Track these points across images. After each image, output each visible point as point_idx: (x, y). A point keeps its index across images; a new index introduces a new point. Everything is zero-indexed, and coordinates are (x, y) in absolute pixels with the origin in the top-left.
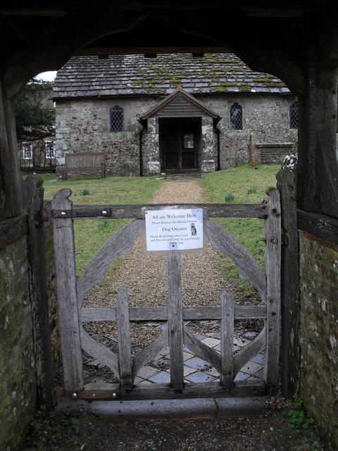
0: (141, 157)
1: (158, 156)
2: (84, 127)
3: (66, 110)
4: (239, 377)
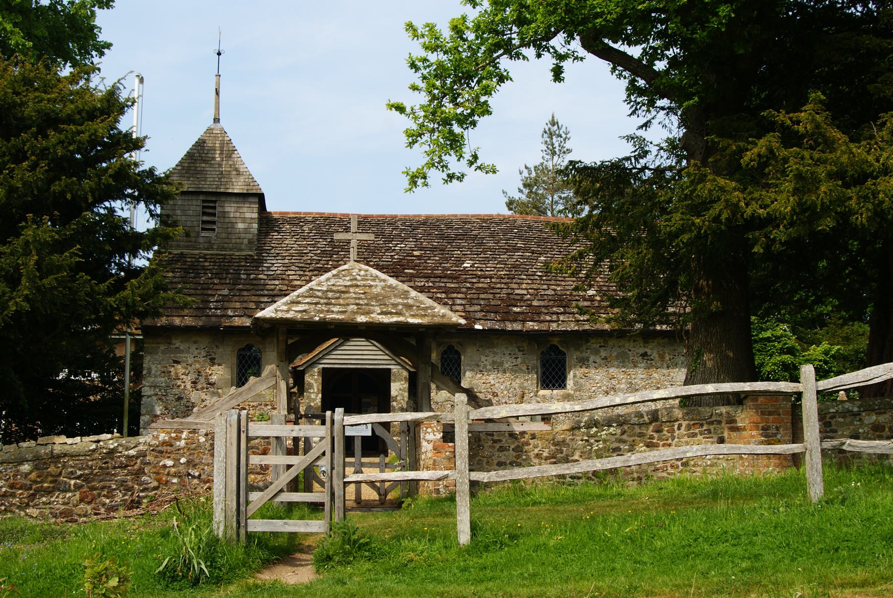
3: (162, 347)
4: (389, 497)
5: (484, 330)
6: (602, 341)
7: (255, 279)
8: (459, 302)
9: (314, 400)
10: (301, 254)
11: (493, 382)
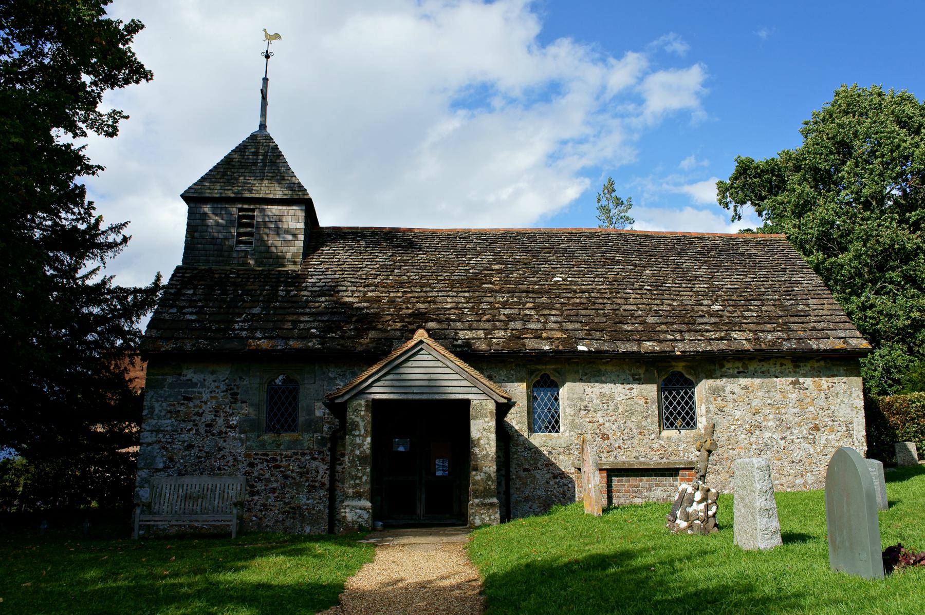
0: (332, 490)
1: (367, 487)
2: (208, 417)
3: (170, 379)
5: (589, 352)
6: (740, 365)
7: (295, 296)
8: (553, 319)
9: (360, 446)
10: (356, 269)
11: (601, 421)
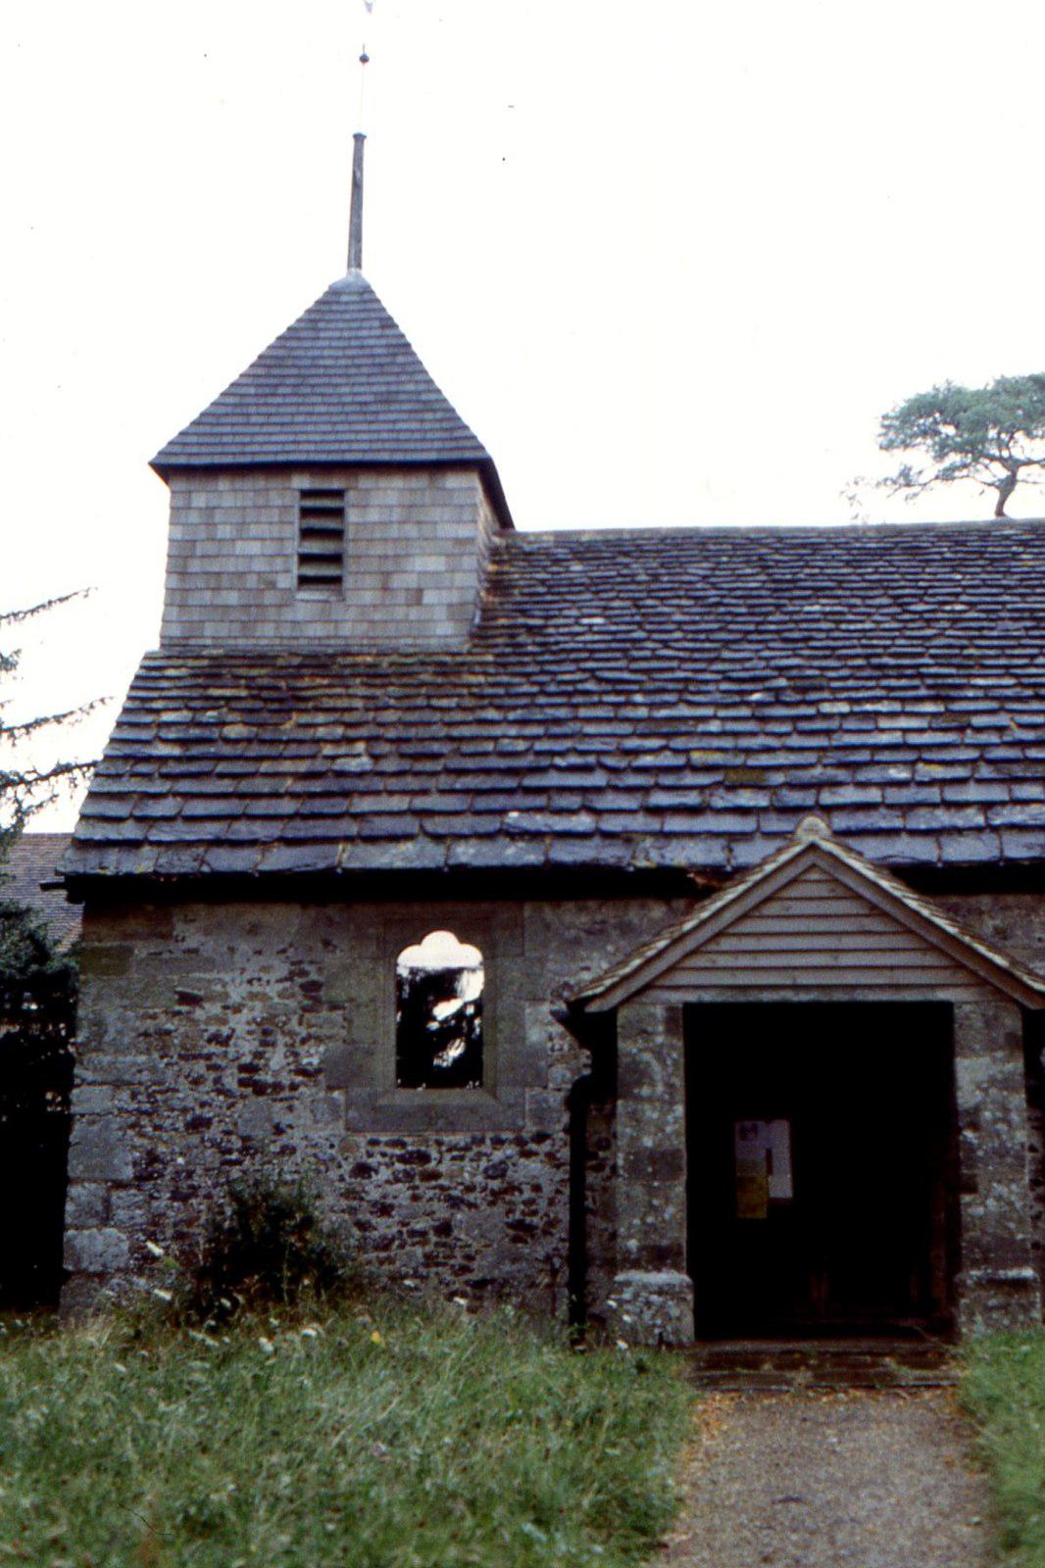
3: (141, 950)
